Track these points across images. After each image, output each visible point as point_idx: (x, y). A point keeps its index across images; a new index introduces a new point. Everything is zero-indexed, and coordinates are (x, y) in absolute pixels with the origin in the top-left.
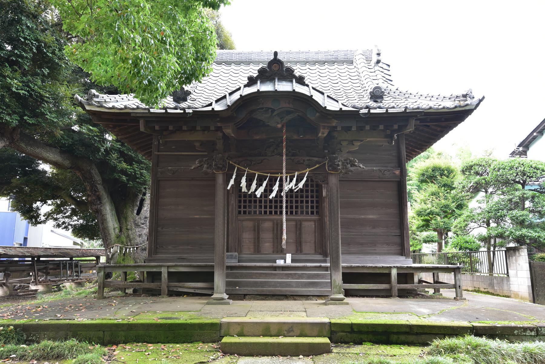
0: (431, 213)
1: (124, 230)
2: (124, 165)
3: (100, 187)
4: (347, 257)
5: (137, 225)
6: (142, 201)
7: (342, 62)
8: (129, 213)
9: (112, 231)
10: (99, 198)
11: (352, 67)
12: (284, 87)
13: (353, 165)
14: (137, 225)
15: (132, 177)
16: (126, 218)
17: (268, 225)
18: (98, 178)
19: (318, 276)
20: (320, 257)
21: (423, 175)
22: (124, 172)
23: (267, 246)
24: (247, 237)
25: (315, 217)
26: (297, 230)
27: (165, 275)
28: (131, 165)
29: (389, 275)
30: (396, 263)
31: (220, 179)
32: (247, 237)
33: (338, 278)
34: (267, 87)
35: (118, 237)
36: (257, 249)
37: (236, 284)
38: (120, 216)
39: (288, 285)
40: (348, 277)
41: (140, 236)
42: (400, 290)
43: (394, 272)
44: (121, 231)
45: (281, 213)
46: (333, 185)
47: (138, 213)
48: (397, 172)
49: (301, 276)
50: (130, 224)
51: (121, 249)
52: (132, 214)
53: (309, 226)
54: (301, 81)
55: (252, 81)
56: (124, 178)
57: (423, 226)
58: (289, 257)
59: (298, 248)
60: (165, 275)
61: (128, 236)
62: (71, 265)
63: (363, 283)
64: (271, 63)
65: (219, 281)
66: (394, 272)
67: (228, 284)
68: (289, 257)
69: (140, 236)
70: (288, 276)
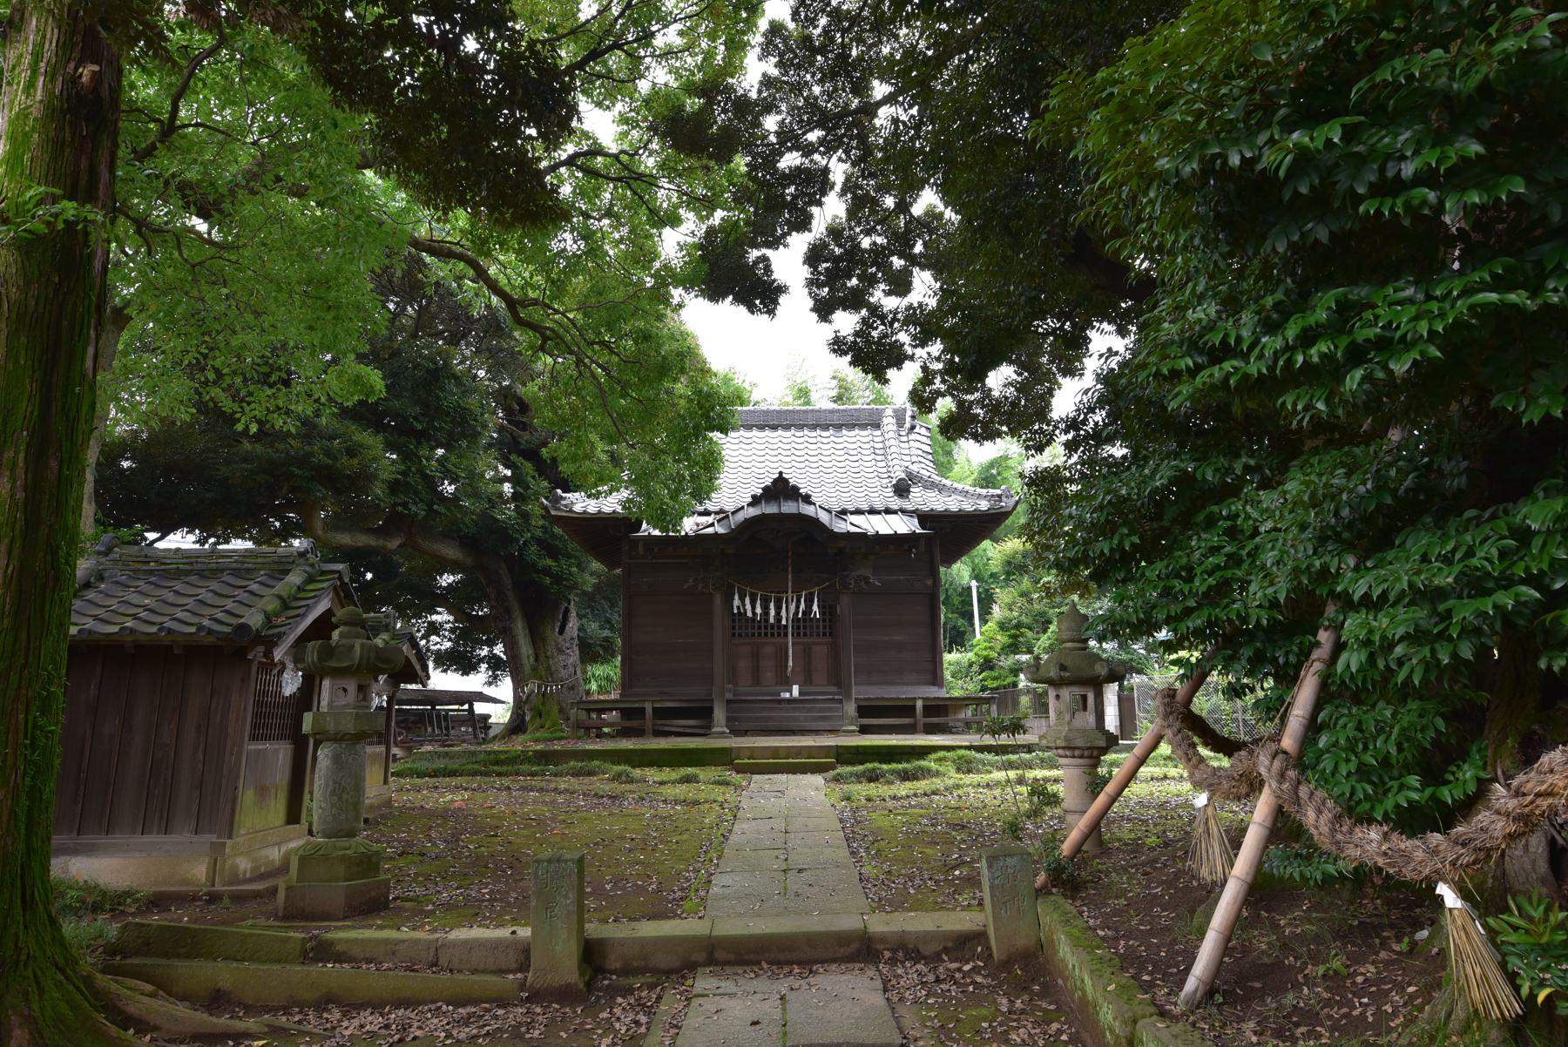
0: (1018, 626)
1: (542, 658)
2: (549, 562)
3: (510, 594)
4: (862, 688)
5: (560, 651)
6: (567, 611)
7: (863, 427)
8: (549, 632)
9: (525, 661)
10: (508, 611)
11: (878, 433)
12: (788, 507)
13: (867, 582)
14: (560, 651)
15: (558, 579)
16: (544, 640)
17: (769, 650)
18: (507, 581)
19: (830, 709)
20: (833, 689)
21: (1009, 563)
22: (547, 571)
23: (769, 676)
24: (744, 665)
25: (828, 639)
26: (805, 656)
27: (649, 711)
28: (556, 559)
29: (914, 707)
30: (921, 693)
31: (718, 601)
32: (744, 665)
33: (851, 709)
34: (771, 509)
35: (534, 669)
36: (757, 681)
37: (736, 719)
38: (536, 638)
39: (797, 719)
40: (864, 711)
41: (565, 667)
42: (926, 725)
43: (919, 704)
44: (537, 660)
45: (786, 635)
46: (844, 605)
47: (561, 631)
48: (929, 582)
49: (809, 710)
50: (551, 650)
51: (539, 687)
52: (552, 633)
53: (821, 651)
54: (807, 499)
55: (755, 501)
56: (548, 581)
57: (1010, 646)
58: (796, 690)
59: (807, 681)
60: (649, 711)
61: (548, 668)
62: (430, 718)
63: (873, 714)
64: (775, 481)
65: (719, 714)
66: (919, 704)
67: (729, 719)
68: (796, 690)
69: (565, 667)
70: (795, 710)
